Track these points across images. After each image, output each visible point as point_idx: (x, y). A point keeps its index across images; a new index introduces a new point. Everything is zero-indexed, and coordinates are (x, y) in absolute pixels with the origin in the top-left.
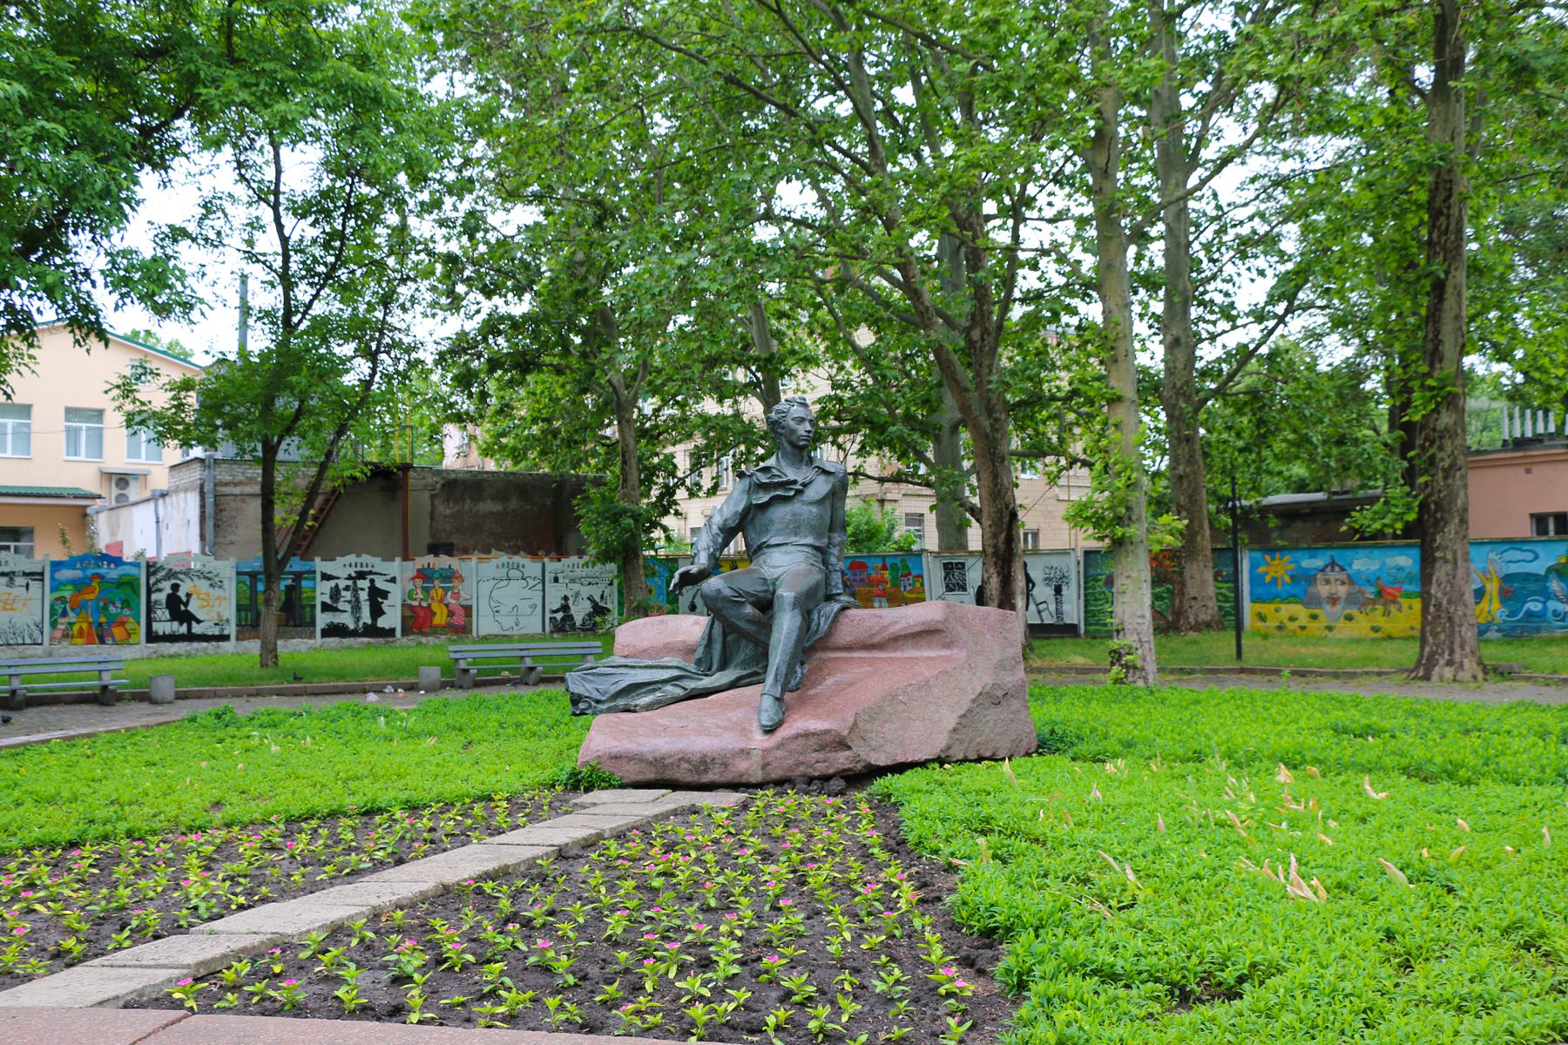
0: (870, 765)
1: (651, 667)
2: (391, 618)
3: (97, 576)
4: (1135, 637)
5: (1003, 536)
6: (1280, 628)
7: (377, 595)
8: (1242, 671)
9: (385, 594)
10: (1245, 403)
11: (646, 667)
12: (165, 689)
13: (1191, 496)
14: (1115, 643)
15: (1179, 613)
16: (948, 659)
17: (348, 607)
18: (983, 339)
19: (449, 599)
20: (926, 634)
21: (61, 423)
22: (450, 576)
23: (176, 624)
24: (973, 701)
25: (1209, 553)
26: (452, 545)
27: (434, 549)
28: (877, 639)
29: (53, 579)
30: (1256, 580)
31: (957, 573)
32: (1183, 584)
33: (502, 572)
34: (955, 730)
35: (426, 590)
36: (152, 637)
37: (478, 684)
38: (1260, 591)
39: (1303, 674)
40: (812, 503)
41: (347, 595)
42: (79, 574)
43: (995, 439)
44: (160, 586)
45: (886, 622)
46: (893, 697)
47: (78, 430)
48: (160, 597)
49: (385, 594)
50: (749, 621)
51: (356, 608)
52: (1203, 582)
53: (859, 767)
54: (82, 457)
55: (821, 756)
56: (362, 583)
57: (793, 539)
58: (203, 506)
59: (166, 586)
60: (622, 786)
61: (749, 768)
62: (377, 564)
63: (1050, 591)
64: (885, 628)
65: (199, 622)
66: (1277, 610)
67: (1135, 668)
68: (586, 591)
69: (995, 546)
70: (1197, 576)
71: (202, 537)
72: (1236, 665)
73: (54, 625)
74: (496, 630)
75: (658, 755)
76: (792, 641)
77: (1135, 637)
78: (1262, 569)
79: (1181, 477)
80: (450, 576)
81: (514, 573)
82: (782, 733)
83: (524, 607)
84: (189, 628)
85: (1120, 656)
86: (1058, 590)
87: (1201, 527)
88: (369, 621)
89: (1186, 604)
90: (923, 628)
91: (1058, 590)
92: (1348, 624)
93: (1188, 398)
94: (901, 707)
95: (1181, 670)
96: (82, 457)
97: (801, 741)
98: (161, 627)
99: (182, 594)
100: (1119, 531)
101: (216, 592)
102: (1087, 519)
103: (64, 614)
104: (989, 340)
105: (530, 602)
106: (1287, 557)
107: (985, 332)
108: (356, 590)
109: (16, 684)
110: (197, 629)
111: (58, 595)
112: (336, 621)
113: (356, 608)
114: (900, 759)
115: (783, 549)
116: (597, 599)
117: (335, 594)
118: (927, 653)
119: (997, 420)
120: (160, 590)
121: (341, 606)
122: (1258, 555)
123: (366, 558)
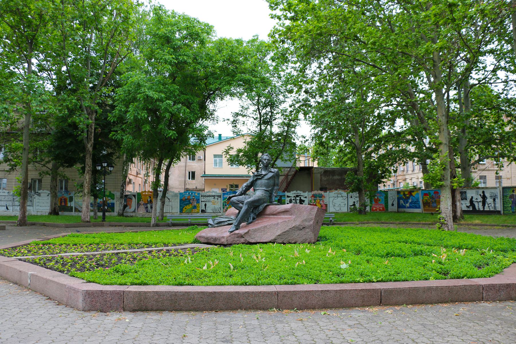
4: (445, 215)
19: (321, 202)
20: (285, 212)
22: (321, 196)
27: (321, 189)
28: (275, 213)
31: (464, 194)
33: (336, 195)
34: (279, 235)
46: (266, 227)
55: (238, 239)
56: (297, 198)
61: (224, 241)
62: (301, 193)
63: (492, 200)
64: (276, 210)
73: (223, 208)
74: (334, 211)
77: (445, 215)
80: (321, 196)
81: (339, 195)
83: (342, 205)
86: (494, 200)
91: (494, 200)
95: (506, 226)
103: (226, 206)
108: (296, 200)
114: (258, 241)
123: (298, 192)
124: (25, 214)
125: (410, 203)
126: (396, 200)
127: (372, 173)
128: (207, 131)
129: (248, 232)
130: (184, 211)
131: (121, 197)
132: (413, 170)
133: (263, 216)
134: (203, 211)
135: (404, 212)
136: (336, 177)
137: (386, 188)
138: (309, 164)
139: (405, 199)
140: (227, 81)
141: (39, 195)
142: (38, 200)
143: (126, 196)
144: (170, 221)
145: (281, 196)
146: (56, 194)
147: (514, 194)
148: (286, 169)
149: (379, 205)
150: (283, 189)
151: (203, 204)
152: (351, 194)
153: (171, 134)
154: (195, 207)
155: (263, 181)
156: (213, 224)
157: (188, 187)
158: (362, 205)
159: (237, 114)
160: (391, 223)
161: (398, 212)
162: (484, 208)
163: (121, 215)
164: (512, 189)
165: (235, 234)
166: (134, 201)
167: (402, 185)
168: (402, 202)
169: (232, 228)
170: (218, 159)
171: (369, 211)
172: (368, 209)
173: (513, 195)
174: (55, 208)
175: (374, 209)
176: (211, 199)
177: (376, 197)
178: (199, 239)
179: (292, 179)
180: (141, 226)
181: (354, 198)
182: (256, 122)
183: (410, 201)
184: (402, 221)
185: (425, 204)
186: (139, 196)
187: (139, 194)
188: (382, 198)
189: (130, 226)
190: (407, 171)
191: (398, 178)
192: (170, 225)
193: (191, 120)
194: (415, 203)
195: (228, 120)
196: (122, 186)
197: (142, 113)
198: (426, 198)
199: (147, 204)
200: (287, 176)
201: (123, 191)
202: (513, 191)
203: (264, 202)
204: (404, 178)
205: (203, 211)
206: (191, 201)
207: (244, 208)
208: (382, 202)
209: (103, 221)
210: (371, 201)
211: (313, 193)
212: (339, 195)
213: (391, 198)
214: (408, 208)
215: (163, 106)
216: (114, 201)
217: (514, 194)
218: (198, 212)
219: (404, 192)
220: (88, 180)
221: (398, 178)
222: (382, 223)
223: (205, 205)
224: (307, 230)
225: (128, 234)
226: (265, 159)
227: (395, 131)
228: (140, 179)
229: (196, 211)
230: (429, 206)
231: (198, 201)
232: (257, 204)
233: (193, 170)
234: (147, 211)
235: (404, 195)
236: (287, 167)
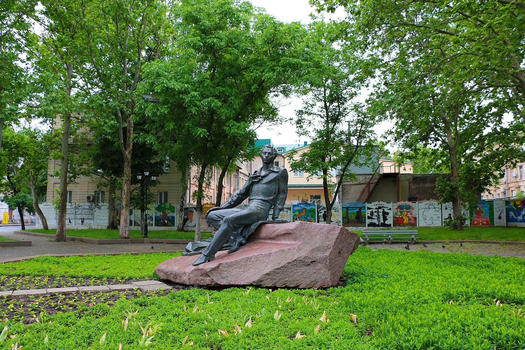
0: (217, 284)
2: (390, 221)
7: (385, 214)
9: (388, 214)
17: (376, 218)
19: (409, 215)
20: (287, 235)
22: (409, 208)
26: (416, 197)
27: (410, 200)
28: (272, 236)
29: (293, 209)
34: (267, 274)
35: (401, 212)
37: (393, 243)
41: (376, 214)
44: (321, 211)
45: (275, 229)
48: (321, 214)
49: (388, 214)
51: (379, 218)
56: (380, 210)
61: (185, 279)
74: (425, 225)
80: (409, 208)
83: (435, 218)
88: (383, 222)
96: (298, 176)
97: (197, 272)
101: (337, 213)
105: (437, 216)
108: (378, 212)
111: (295, 214)
112: (372, 222)
113: (379, 218)
114: (232, 283)
117: (372, 213)
118: (288, 242)
120: (321, 213)
121: (374, 217)
123: (381, 202)
124: (63, 229)
127: (471, 179)
129: (218, 267)
131: (181, 210)
133: (258, 241)
135: (516, 227)
136: (428, 185)
137: (491, 198)
138: (395, 170)
141: (99, 208)
142: (99, 214)
143: (186, 209)
145: (360, 208)
146: (114, 206)
148: (368, 177)
149: (482, 217)
152: (443, 205)
153: (199, 133)
158: (457, 219)
159: (300, 112)
160: (494, 243)
161: (507, 226)
163: (181, 230)
167: (515, 194)
168: (512, 214)
171: (469, 225)
172: (468, 222)
174: (113, 221)
175: (476, 222)
177: (478, 209)
179: (374, 188)
181: (448, 210)
184: (510, 240)
188: (485, 209)
189: (172, 243)
190: (521, 177)
191: (510, 185)
196: (182, 198)
200: (369, 184)
201: (183, 203)
203: (259, 219)
204: (517, 185)
207: (223, 227)
208: (485, 213)
209: (144, 237)
210: (471, 213)
211: (399, 203)
212: (430, 206)
213: (498, 209)
214: (521, 221)
215: (187, 99)
216: (174, 215)
219: (514, 201)
220: (126, 191)
221: (510, 185)
222: (482, 242)
224: (319, 266)
226: (266, 153)
227: (501, 128)
236: (368, 175)
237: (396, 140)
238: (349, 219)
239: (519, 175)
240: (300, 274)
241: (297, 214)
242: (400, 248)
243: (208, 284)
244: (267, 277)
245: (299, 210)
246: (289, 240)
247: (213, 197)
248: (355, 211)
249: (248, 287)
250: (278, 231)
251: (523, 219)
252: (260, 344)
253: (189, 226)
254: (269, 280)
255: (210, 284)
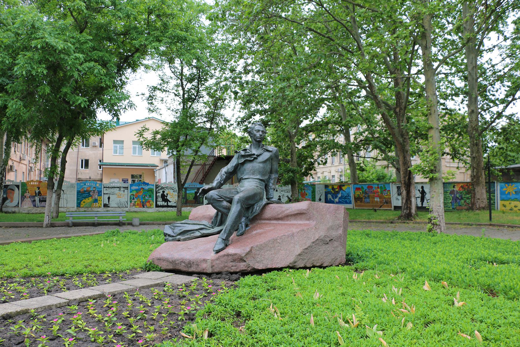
1: (195, 224)
3: (142, 188)
4: (437, 214)
5: (407, 177)
6: (511, 210)
8: (491, 225)
10: (501, 132)
11: (193, 224)
12: (136, 222)
13: (478, 164)
14: (429, 216)
15: (473, 204)
16: (305, 225)
18: (400, 111)
20: (299, 214)
21: (112, 145)
23: (164, 202)
24: (313, 243)
25: (484, 184)
28: (280, 216)
29: (130, 189)
30: (502, 193)
32: (475, 194)
34: (299, 255)
36: (157, 206)
38: (504, 196)
39: (512, 227)
40: (260, 163)
42: (137, 188)
43: (404, 145)
45: (284, 209)
46: (275, 240)
47: (136, 147)
48: (159, 195)
50: (224, 208)
52: (482, 193)
53: (249, 269)
54: (155, 155)
55: (234, 264)
57: (252, 176)
58: (174, 168)
59: (161, 191)
60: (161, 271)
61: (207, 267)
64: (283, 212)
65: (170, 202)
66: (510, 203)
67: (437, 225)
68: (286, 194)
69: (405, 181)
70: (480, 191)
71: (174, 177)
72: (489, 223)
73: (131, 202)
75: (173, 259)
76: (234, 216)
78: (504, 189)
79: (474, 158)
82: (221, 253)
84: (167, 203)
85: (431, 220)
87: (481, 174)
89: (476, 201)
90: (298, 212)
92: (6, 252)
93: (477, 130)
94: (278, 244)
95: (468, 224)
96: (155, 155)
97: (226, 257)
98: (159, 203)
99: (165, 194)
100: (431, 175)
102: (419, 171)
103: (134, 199)
104: (402, 111)
106: (514, 185)
107: (401, 109)
109: (121, 218)
110: (169, 204)
111: (132, 193)
115: (247, 180)
116: (290, 197)
119: (405, 138)
122: (503, 184)
125: (340, 198)
126: (324, 194)
128: (127, 101)
130: (81, 206)
132: (332, 163)
133: (260, 222)
134: (105, 206)
139: (334, 194)
140: (157, 37)
143: (6, 186)
144: (70, 220)
147: (455, 189)
150: (199, 180)
151: (106, 197)
153: (79, 102)
154: (96, 201)
155: (256, 165)
156: (172, 234)
157: (80, 176)
159: (155, 89)
162: (422, 204)
164: (453, 185)
165: (228, 255)
166: (17, 194)
168: (330, 196)
169: (216, 241)
170: (118, 145)
173: (454, 190)
176: (116, 191)
178: (156, 263)
180: (29, 227)
182: (179, 100)
183: (340, 195)
185: (357, 199)
186: (23, 187)
187: (24, 185)
192: (71, 225)
193: (107, 85)
194: (345, 198)
195: (143, 94)
197: (38, 67)
198: (358, 193)
199: (34, 197)
200: (205, 165)
202: (454, 187)
205: (105, 206)
206: (91, 193)
213: (319, 192)
217: (455, 189)
218: (100, 207)
219: (333, 186)
223: (109, 198)
224: (336, 244)
225: (17, 247)
226: (259, 131)
228: (24, 166)
229: (97, 205)
230: (361, 202)
231: (100, 193)
232: (251, 202)
233: (87, 158)
234: (35, 206)
235: (333, 189)
237: (238, 124)
238: (187, 200)
239: (233, 162)
240: (322, 252)
241: (134, 193)
242: (36, 228)
243: (243, 270)
244: (299, 257)
245: (136, 190)
246: (301, 220)
247: (25, 174)
248: (193, 192)
249: (285, 269)
250: (288, 211)
251: (339, 201)
252: (320, 325)
253: (8, 207)
254: (301, 260)
255: (245, 270)
